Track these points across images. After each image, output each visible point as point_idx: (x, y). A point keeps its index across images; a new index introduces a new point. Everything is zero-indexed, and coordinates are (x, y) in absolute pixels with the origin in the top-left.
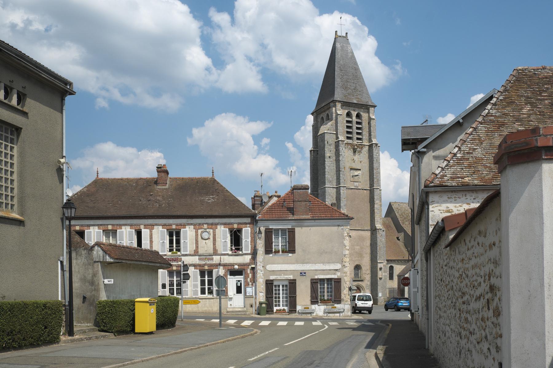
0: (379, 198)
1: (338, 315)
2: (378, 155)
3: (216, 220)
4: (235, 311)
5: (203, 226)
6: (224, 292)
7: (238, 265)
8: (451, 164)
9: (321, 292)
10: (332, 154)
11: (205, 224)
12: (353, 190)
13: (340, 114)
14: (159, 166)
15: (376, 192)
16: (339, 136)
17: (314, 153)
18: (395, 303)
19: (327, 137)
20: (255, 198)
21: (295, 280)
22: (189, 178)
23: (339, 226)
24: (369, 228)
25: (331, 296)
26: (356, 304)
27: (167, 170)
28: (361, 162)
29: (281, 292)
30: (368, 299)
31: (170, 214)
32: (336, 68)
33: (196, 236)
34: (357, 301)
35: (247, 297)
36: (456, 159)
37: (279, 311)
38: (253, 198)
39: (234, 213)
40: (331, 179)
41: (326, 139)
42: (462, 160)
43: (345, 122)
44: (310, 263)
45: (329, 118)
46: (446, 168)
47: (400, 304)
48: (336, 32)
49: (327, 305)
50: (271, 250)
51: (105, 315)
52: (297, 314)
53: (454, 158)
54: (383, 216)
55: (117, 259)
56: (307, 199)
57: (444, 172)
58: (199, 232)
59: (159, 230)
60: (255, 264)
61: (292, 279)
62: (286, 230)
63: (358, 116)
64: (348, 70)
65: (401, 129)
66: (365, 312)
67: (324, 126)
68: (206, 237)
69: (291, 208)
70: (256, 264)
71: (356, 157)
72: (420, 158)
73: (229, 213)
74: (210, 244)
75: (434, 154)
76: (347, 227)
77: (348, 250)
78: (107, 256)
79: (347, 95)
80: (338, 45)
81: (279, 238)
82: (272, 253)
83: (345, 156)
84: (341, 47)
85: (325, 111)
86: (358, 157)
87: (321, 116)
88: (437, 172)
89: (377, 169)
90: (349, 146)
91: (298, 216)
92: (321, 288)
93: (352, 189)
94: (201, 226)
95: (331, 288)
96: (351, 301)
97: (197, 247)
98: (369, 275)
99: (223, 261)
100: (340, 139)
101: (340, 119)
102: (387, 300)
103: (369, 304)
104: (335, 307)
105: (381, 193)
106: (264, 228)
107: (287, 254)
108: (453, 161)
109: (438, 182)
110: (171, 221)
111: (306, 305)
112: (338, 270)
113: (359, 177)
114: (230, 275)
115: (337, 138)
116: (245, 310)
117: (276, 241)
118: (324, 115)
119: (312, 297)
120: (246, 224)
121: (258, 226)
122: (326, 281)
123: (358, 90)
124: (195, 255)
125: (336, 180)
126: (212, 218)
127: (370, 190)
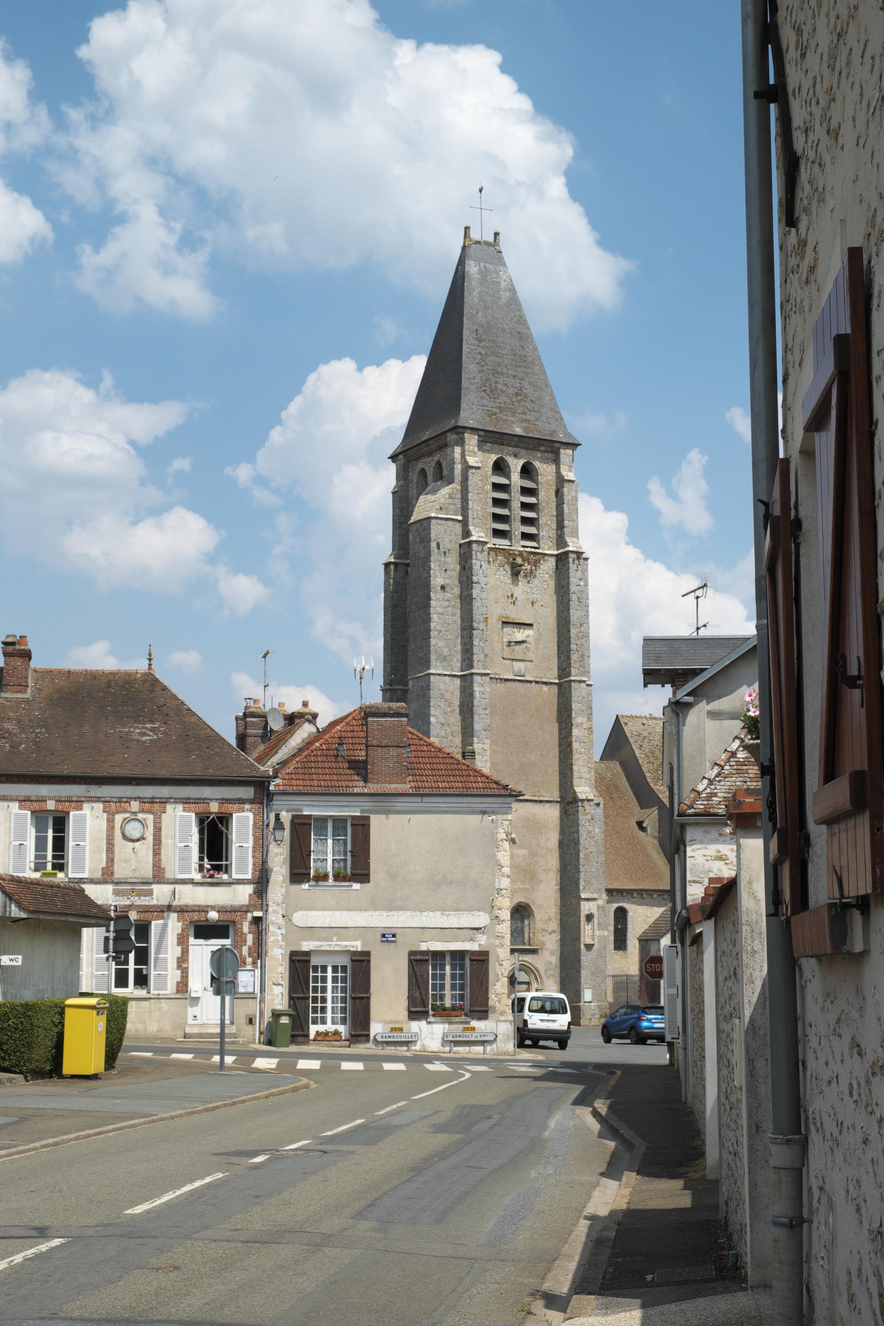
0: (584, 708)
1: (479, 1049)
2: (582, 583)
3: (164, 791)
4: (207, 1034)
5: (127, 804)
6: (232, 985)
7: (218, 911)
8: (726, 772)
9: (434, 987)
10: (450, 578)
11: (135, 799)
12: (509, 684)
13: (476, 465)
14: (10, 640)
15: (578, 693)
16: (471, 528)
17: (396, 570)
18: (631, 1022)
19: (436, 530)
20: (248, 719)
21: (367, 954)
22: (86, 670)
23: (484, 813)
24: (556, 796)
25: (462, 998)
26: (525, 1022)
27: (30, 651)
28: (533, 603)
29: (329, 984)
30: (557, 1008)
31: (43, 771)
32: (466, 334)
33: (108, 830)
34: (527, 1014)
35: (239, 996)
36: (734, 763)
37: (322, 1037)
38: (241, 719)
39: (211, 773)
40: (446, 650)
41: (432, 536)
42: (746, 765)
43: (489, 487)
44: (408, 910)
45: (442, 475)
46: (717, 779)
47: (645, 1024)
48: (467, 229)
49: (450, 1023)
50: (305, 871)
51: (7, 1035)
52: (370, 1045)
53: (732, 760)
54: (597, 758)
55: (32, 912)
56: (402, 742)
57: (713, 787)
58: (116, 821)
59: (10, 813)
60: (264, 907)
61: (359, 949)
62: (346, 820)
63: (527, 471)
64: (500, 339)
65: (642, 642)
66: (549, 1043)
67: (429, 497)
68: (136, 835)
69: (359, 761)
70: (265, 908)
71: (521, 589)
72: (681, 714)
73: (198, 773)
74: (145, 852)
75: (710, 707)
76: (505, 817)
77: (508, 877)
78: (13, 905)
79: (495, 410)
80: (472, 268)
81: (326, 840)
82: (309, 881)
83: (489, 586)
84: (480, 272)
85: (430, 454)
86: (527, 588)
87: (420, 465)
88: (700, 787)
89: (581, 625)
90: (500, 558)
91: (379, 786)
92: (434, 977)
93: (507, 680)
94: (123, 805)
95: (462, 977)
96: (513, 1012)
97: (110, 860)
98: (554, 935)
99: (179, 900)
100: (473, 538)
101: (474, 479)
102: (608, 1012)
103: (561, 1021)
104: (473, 1029)
105: (590, 694)
106: (290, 814)
107: (349, 884)
108: (730, 766)
109: (702, 807)
110: (43, 790)
111: (395, 1022)
112: (480, 929)
113: (527, 647)
114: (197, 936)
115: (467, 533)
116: (234, 1031)
117: (320, 848)
118: (428, 464)
119: (412, 1000)
120: (242, 801)
121: (274, 807)
122: (448, 959)
123: (526, 396)
124: (104, 882)
125: (462, 654)
126: (154, 785)
127: (559, 685)
